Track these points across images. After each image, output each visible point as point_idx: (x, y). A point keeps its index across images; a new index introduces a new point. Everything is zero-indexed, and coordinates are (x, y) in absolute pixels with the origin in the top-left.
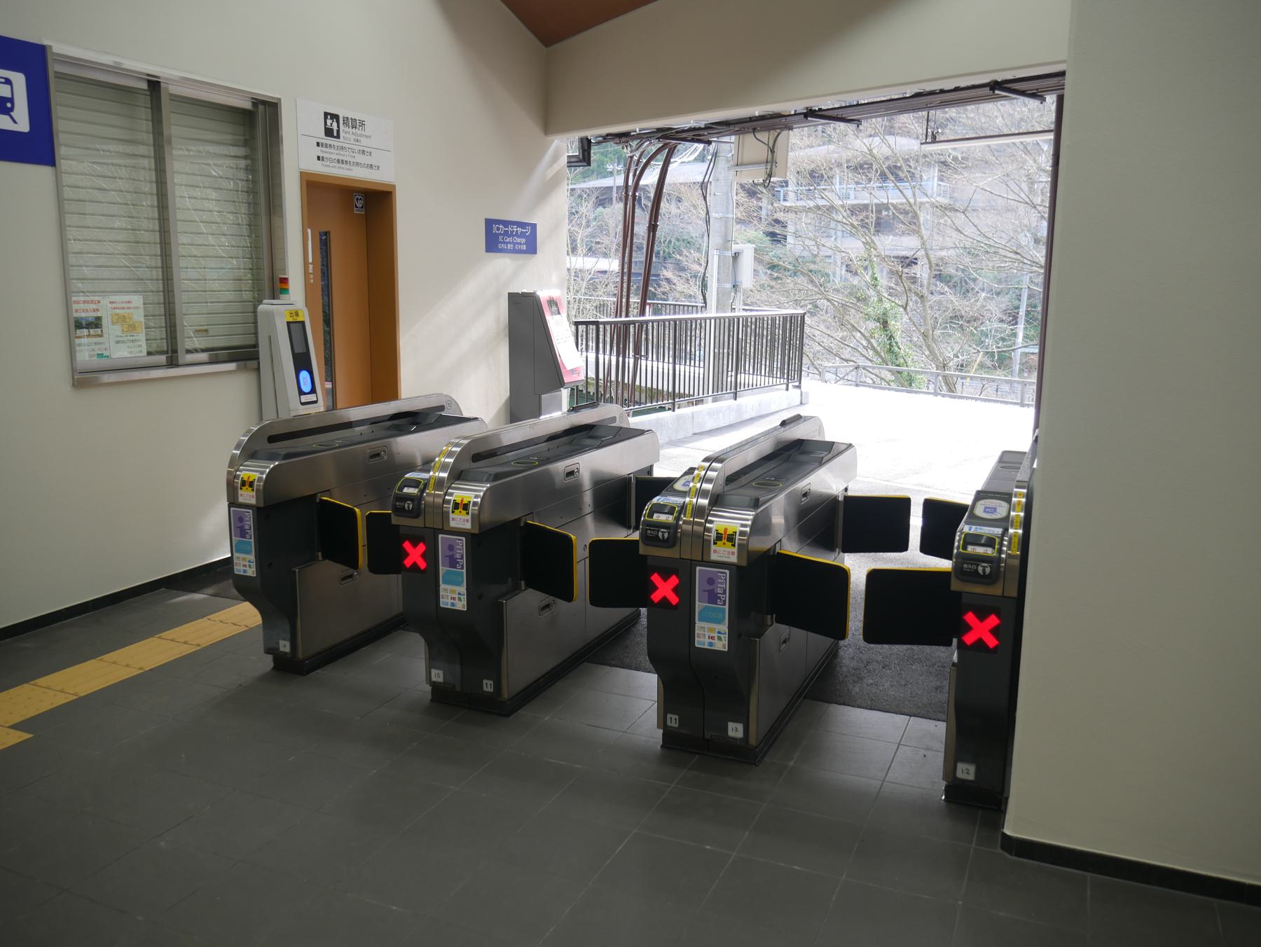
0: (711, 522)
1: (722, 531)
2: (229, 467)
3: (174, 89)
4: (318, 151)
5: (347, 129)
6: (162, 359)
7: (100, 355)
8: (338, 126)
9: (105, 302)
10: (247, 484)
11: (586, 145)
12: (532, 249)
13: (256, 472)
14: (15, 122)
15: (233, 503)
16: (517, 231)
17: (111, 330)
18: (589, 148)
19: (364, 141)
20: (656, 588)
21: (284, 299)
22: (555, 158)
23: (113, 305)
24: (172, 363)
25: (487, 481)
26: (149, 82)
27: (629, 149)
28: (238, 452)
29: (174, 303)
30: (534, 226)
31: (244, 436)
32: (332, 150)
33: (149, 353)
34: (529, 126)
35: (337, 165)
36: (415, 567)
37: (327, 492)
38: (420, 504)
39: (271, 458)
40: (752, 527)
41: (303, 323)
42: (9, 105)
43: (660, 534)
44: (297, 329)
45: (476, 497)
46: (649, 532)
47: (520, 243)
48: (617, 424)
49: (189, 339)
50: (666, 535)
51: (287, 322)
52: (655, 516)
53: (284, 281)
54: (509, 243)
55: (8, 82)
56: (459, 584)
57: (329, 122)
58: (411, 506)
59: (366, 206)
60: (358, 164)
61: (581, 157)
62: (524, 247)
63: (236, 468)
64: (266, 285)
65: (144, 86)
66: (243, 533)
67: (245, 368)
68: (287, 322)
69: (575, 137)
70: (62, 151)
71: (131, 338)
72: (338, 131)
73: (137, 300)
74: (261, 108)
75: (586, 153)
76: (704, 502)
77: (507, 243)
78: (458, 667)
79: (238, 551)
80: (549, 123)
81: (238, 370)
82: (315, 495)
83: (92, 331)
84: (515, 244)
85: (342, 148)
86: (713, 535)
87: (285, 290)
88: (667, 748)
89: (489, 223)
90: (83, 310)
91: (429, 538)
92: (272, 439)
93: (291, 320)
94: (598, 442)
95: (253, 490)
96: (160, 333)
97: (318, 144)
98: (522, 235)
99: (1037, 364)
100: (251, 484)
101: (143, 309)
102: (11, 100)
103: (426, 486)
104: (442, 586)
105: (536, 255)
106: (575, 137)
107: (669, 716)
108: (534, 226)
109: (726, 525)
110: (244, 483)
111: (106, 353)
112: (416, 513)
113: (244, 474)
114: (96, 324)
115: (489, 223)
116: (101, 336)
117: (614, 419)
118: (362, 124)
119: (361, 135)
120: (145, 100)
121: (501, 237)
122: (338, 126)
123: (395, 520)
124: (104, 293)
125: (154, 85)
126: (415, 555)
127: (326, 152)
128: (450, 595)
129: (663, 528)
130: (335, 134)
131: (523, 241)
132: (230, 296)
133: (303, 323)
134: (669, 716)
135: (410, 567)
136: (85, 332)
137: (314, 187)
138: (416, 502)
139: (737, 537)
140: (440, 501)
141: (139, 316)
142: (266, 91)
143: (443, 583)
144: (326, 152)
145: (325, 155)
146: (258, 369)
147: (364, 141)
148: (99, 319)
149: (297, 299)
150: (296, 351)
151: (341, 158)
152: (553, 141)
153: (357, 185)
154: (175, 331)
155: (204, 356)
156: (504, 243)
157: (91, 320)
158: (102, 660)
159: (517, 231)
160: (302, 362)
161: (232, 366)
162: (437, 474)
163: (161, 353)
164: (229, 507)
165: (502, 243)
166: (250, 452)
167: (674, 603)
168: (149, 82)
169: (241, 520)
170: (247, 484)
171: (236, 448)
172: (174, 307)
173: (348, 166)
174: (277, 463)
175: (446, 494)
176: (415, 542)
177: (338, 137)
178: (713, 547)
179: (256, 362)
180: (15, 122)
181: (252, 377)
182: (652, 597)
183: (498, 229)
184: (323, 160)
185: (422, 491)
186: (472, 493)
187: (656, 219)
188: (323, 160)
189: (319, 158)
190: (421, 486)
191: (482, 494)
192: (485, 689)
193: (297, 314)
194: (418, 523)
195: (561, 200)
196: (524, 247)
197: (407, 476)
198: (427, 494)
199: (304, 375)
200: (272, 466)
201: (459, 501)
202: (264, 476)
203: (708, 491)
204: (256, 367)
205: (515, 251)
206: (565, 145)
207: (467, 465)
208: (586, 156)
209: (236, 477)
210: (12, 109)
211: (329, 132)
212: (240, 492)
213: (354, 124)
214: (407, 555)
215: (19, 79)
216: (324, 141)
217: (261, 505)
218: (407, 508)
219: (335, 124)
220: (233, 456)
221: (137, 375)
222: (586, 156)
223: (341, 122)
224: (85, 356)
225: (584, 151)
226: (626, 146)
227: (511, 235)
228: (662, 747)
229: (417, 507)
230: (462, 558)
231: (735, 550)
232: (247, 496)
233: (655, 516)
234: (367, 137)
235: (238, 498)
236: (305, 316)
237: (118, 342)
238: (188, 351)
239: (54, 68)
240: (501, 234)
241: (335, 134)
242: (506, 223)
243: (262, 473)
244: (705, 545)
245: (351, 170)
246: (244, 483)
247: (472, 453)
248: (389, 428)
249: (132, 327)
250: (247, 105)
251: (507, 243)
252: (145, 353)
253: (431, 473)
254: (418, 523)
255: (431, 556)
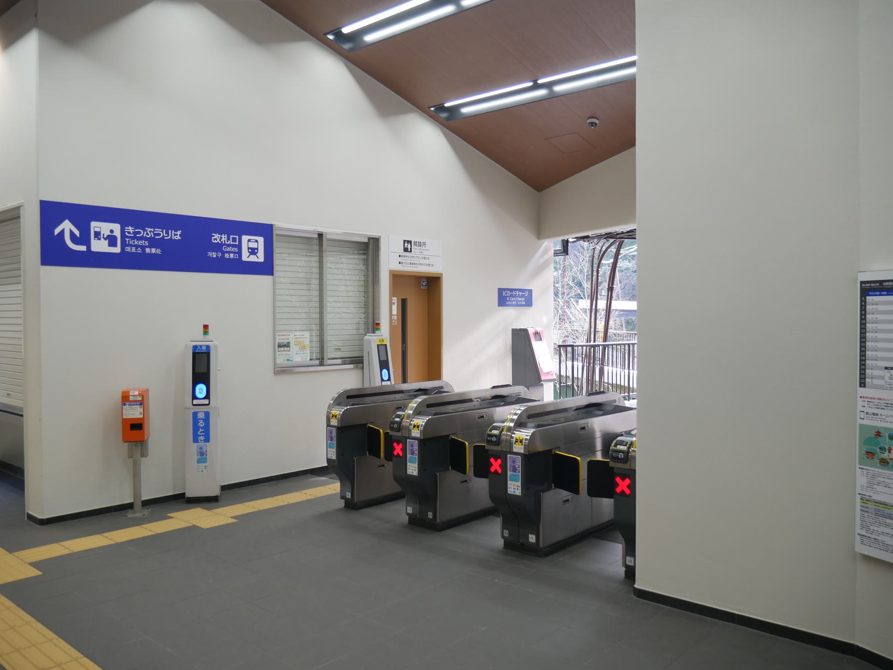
0: (514, 434)
1: (518, 438)
2: (328, 409)
3: (329, 237)
4: (400, 259)
5: (416, 247)
6: (317, 362)
7: (288, 360)
8: (411, 246)
9: (292, 335)
10: (416, 426)
11: (565, 244)
12: (529, 303)
13: (338, 411)
14: (258, 258)
15: (328, 425)
16: (519, 294)
17: (294, 348)
18: (567, 245)
19: (425, 252)
20: (618, 485)
21: (378, 333)
22: (546, 252)
23: (295, 337)
24: (321, 364)
25: (534, 428)
26: (318, 234)
27: (593, 243)
28: (332, 402)
29: (323, 335)
30: (530, 291)
31: (336, 394)
32: (407, 258)
33: (311, 360)
34: (526, 235)
35: (410, 265)
36: (496, 472)
37: (559, 448)
38: (499, 439)
39: (428, 415)
40: (531, 437)
41: (386, 345)
42: (256, 251)
43: (619, 456)
44: (382, 348)
45: (527, 436)
46: (614, 454)
47: (521, 301)
48: (617, 404)
49: (330, 353)
50: (622, 456)
51: (378, 345)
52: (618, 447)
53: (378, 324)
54: (514, 301)
55: (257, 241)
56: (517, 481)
57: (406, 245)
58: (495, 439)
59: (428, 285)
60: (421, 264)
61: (562, 250)
62: (524, 303)
63: (410, 419)
64: (370, 325)
65: (316, 236)
66: (332, 439)
67: (357, 368)
68: (378, 345)
69: (559, 239)
70: (276, 268)
71: (303, 352)
72: (411, 249)
73: (307, 334)
74: (371, 240)
75: (565, 248)
76: (512, 425)
77: (512, 301)
78: (418, 506)
79: (330, 447)
80: (540, 231)
81: (354, 368)
82: (449, 435)
83: (285, 349)
84: (517, 301)
85: (413, 257)
86: (514, 440)
87: (378, 329)
88: (506, 548)
89: (500, 291)
90: (280, 339)
91: (502, 456)
92: (348, 397)
93: (379, 343)
94: (601, 412)
95: (522, 445)
96: (316, 350)
97: (400, 256)
98: (523, 296)
99: (603, 330)
100: (336, 416)
101: (309, 339)
102: (257, 249)
103: (503, 430)
104: (509, 482)
105: (532, 307)
106: (559, 239)
107: (504, 531)
108: (530, 291)
109: (519, 435)
110: (333, 416)
111: (291, 359)
112: (399, 429)
113: (334, 412)
114: (287, 345)
115: (500, 291)
116: (289, 351)
117: (615, 401)
118: (424, 244)
119: (423, 250)
120: (316, 242)
121: (508, 299)
122: (411, 246)
123: (612, 464)
124: (291, 331)
125: (320, 235)
126: (496, 465)
127: (403, 260)
128: (411, 468)
129: (621, 452)
130: (409, 250)
131: (523, 299)
132: (354, 332)
133: (386, 345)
134: (504, 531)
135: (397, 455)
136: (282, 349)
137: (397, 278)
138: (497, 438)
139: (524, 441)
140: (408, 424)
141: (307, 342)
142: (374, 234)
143: (510, 480)
144: (403, 260)
145: (403, 261)
146: (363, 368)
147: (425, 252)
148: (289, 343)
149: (384, 332)
150: (381, 359)
151: (412, 262)
152: (544, 242)
153: (412, 274)
154: (323, 349)
155: (339, 361)
156: (510, 301)
157: (286, 343)
158: (300, 492)
159: (519, 294)
160: (384, 365)
161: (351, 366)
162: (508, 424)
163: (317, 359)
164: (327, 426)
165: (508, 301)
166: (338, 402)
167: (628, 493)
168: (318, 234)
169: (331, 433)
170: (416, 426)
171: (332, 400)
172: (324, 338)
173: (416, 266)
174: (430, 417)
175: (411, 421)
176: (496, 458)
177: (411, 251)
178: (514, 445)
179: (362, 364)
180: (258, 258)
181: (360, 372)
182: (616, 490)
183: (506, 293)
184: (402, 263)
185: (402, 419)
186: (524, 434)
187: (613, 284)
188: (402, 263)
189: (400, 263)
190: (500, 430)
191: (426, 421)
192: (429, 516)
193: (383, 341)
194: (399, 434)
195: (550, 274)
196: (524, 303)
197: (397, 413)
198: (632, 450)
199: (385, 371)
200: (428, 419)
201: (416, 424)
202: (341, 413)
203: (514, 419)
204: (362, 366)
205: (517, 305)
206: (552, 244)
207: (524, 420)
208: (566, 250)
209: (330, 413)
210: (257, 253)
211: (406, 250)
212: (331, 420)
213: (420, 244)
214: (492, 465)
215: (261, 240)
216: (403, 254)
217: (339, 426)
218: (620, 457)
219: (409, 245)
220: (330, 404)
221: (303, 369)
222: (566, 250)
223: (413, 244)
224: (281, 360)
225: (564, 247)
226: (592, 243)
227: (515, 296)
228: (504, 547)
229: (498, 440)
230: (519, 467)
231: (523, 447)
232: (334, 422)
233: (493, 431)
234: (427, 250)
235: (411, 434)
236: (387, 342)
237: (297, 354)
238: (329, 359)
239: (275, 232)
240: (508, 296)
241: (409, 250)
242: (511, 290)
243: (340, 411)
244: (511, 445)
245: (417, 267)
246: (333, 416)
247: (427, 404)
248: (489, 403)
249: (304, 347)
250: (366, 240)
251: (512, 301)
252: (309, 359)
253: (505, 424)
254: (399, 434)
255: (504, 466)
